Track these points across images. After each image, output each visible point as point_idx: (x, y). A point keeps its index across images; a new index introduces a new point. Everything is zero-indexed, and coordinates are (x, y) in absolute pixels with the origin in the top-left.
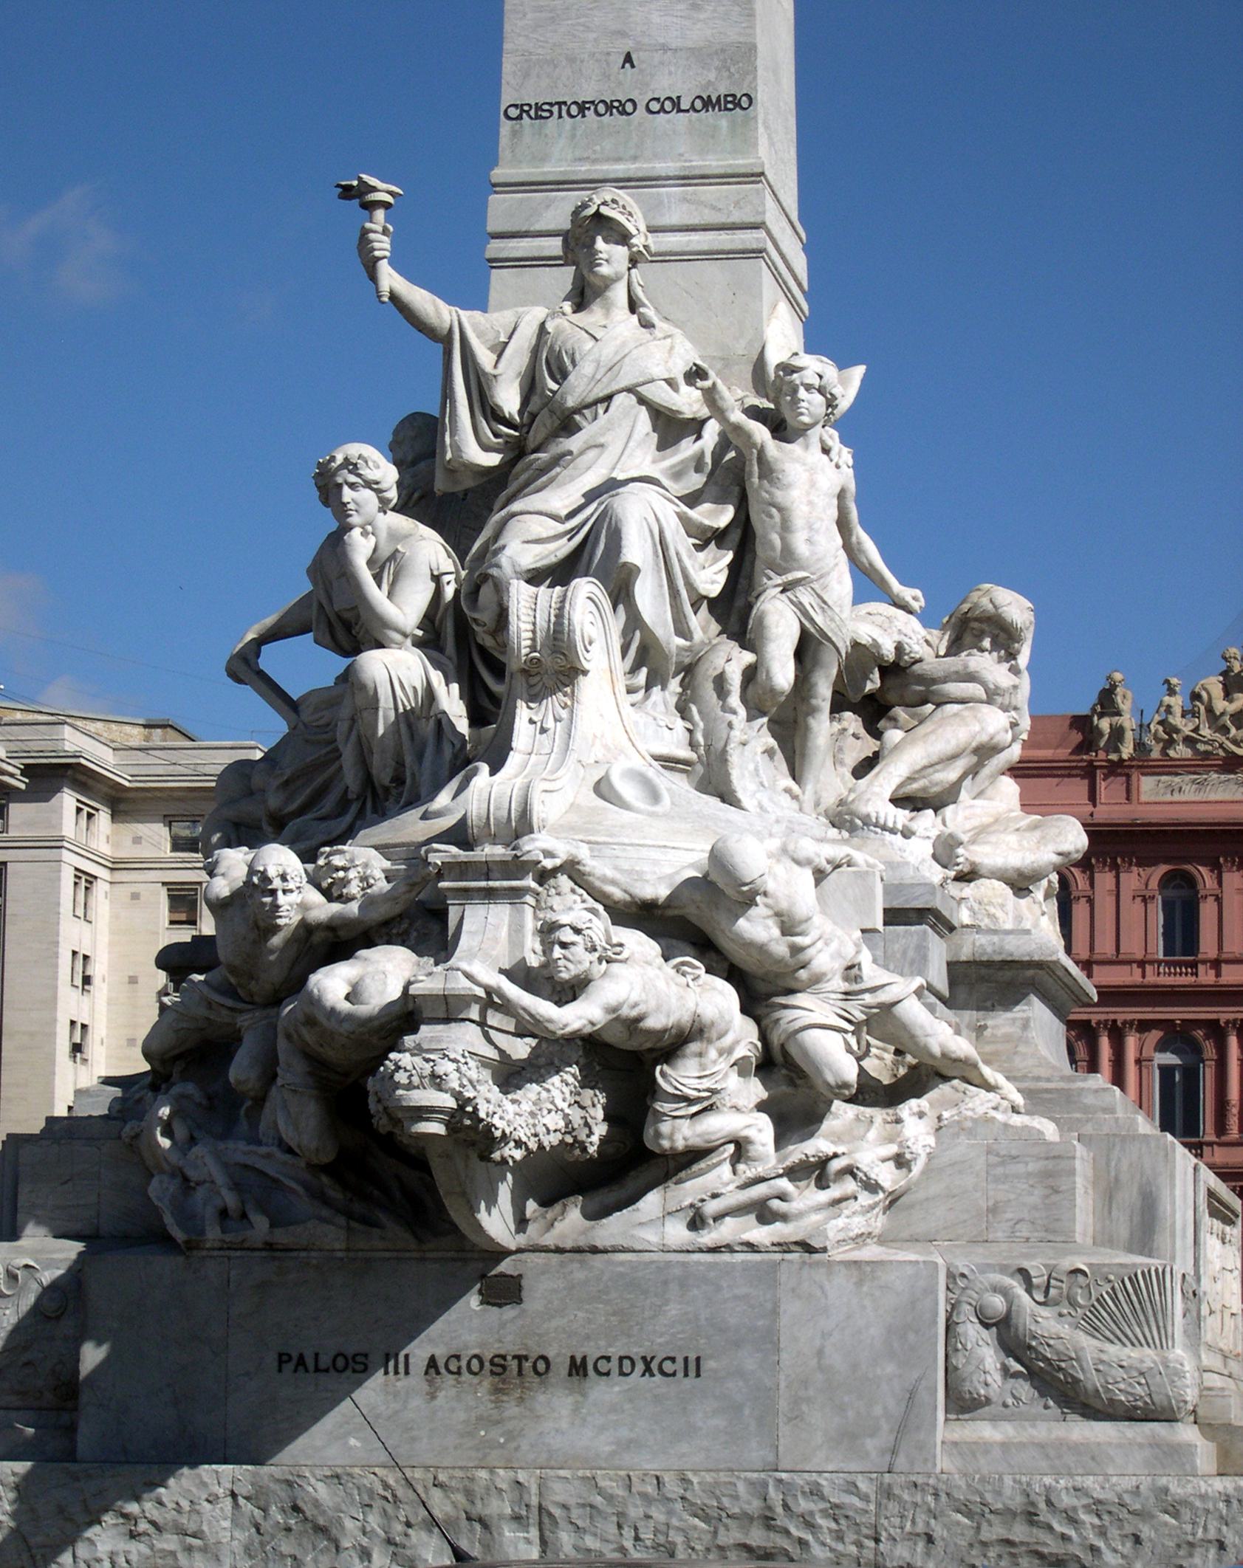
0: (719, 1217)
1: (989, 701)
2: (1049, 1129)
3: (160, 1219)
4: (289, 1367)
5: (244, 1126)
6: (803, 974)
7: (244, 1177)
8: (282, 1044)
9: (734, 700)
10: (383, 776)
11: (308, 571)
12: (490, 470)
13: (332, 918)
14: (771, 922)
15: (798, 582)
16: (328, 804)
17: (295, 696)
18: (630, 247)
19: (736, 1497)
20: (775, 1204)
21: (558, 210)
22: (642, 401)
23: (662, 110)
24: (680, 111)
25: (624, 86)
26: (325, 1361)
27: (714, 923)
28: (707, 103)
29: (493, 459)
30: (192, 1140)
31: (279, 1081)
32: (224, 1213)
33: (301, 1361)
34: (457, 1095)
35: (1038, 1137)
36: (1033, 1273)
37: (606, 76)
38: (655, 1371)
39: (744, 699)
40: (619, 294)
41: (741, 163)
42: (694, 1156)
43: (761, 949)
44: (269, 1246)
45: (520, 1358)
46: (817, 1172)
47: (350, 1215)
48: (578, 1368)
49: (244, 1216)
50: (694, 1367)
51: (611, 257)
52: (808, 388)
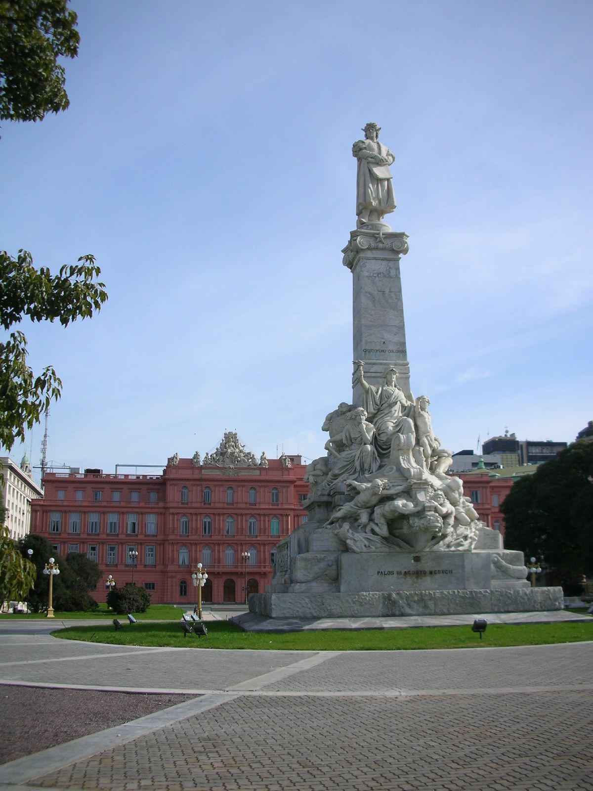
4: (379, 574)
19: (467, 594)
26: (386, 573)
37: (380, 345)
43: (456, 498)
45: (421, 571)
50: (451, 572)
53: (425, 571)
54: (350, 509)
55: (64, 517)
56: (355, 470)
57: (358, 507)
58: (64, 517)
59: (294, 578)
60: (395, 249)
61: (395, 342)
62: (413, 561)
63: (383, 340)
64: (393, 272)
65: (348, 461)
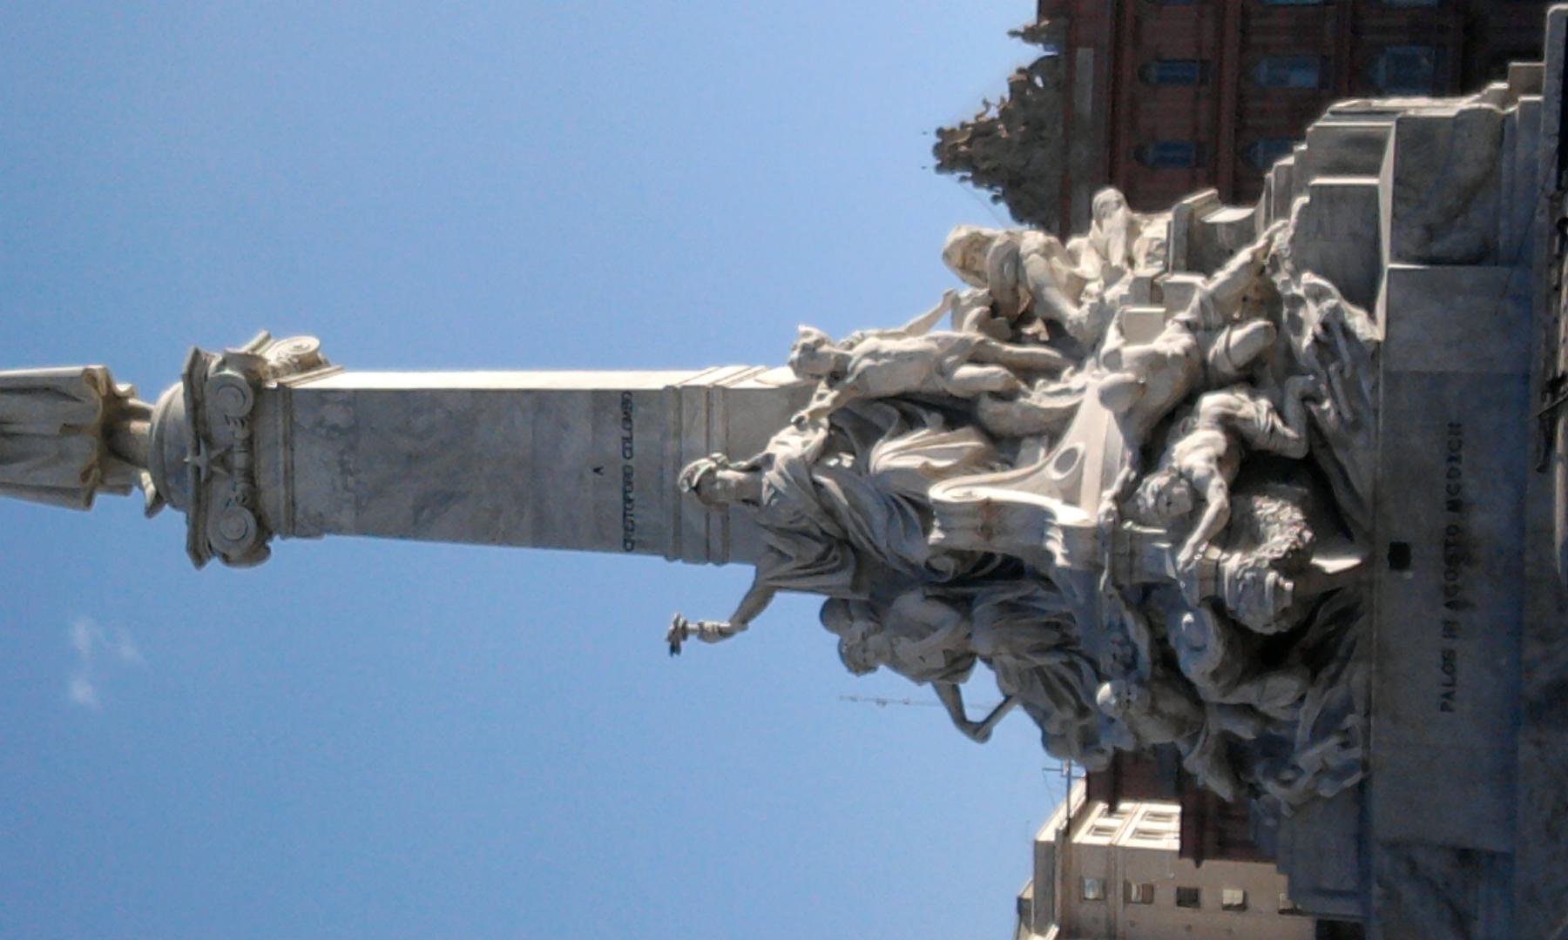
2: (1301, 201)
3: (1346, 790)
5: (1284, 733)
7: (1321, 731)
8: (1232, 700)
10: (1053, 637)
11: (920, 685)
16: (1070, 676)
17: (1002, 699)
23: (631, 449)
24: (631, 438)
28: (627, 419)
30: (1295, 768)
31: (1255, 702)
32: (1345, 745)
33: (1448, 696)
35: (1305, 208)
44: (1367, 714)
45: (1447, 545)
47: (1347, 659)
48: (1454, 506)
49: (1346, 731)
50: (1455, 428)
53: (1448, 529)
60: (247, 409)
61: (594, 429)
62: (1409, 575)
63: (590, 476)
64: (336, 416)
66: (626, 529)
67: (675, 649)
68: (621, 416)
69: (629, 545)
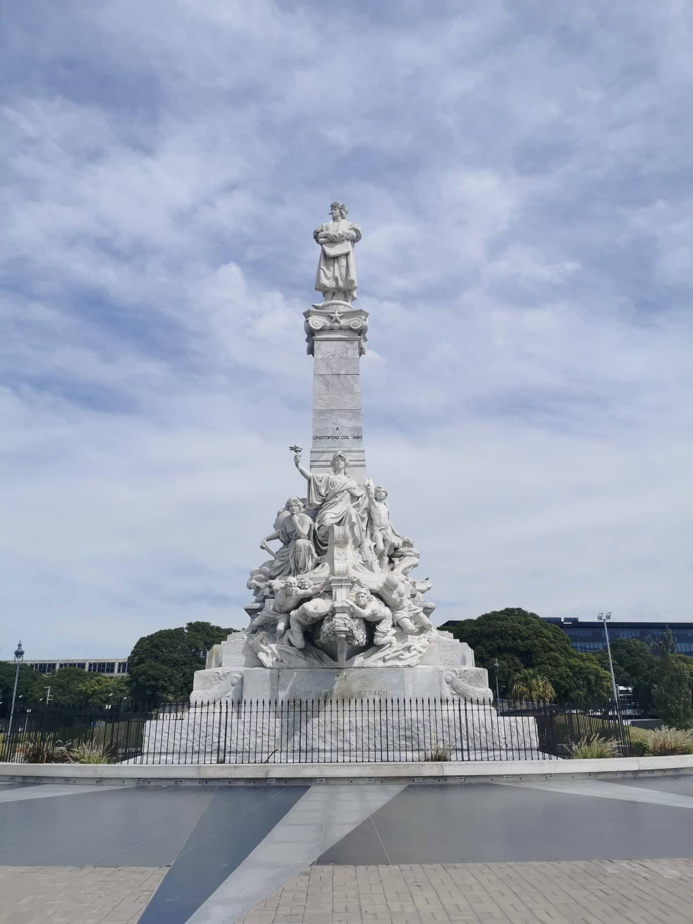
0: (389, 660)
1: (415, 556)
6: (402, 606)
9: (373, 552)
12: (318, 505)
13: (304, 593)
14: (397, 594)
15: (383, 529)
18: (345, 462)
20: (401, 656)
21: (330, 457)
22: (349, 492)
25: (337, 434)
27: (386, 595)
29: (319, 503)
34: (349, 628)
36: (457, 671)
37: (333, 432)
38: (377, 694)
39: (375, 551)
40: (343, 471)
41: (361, 449)
42: (383, 646)
46: (408, 649)
51: (342, 464)
52: (383, 491)
54: (268, 615)
55: (592, 737)
56: (290, 570)
57: (276, 611)
58: (592, 737)
59: (520, 748)
65: (284, 560)
66: (320, 437)
67: (292, 448)
68: (481, 873)
69: (315, 438)
